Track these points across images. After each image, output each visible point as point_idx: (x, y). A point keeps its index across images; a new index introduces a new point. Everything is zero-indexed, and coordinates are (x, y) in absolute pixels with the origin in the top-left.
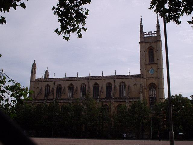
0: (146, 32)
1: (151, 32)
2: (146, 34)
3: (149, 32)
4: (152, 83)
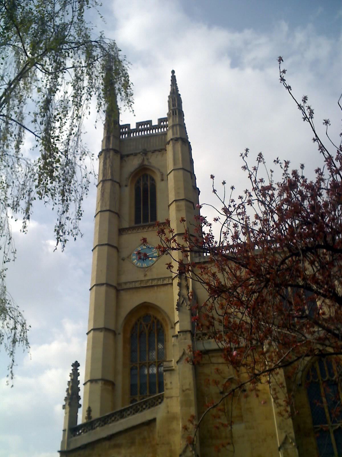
1: (150, 122)
4: (146, 306)
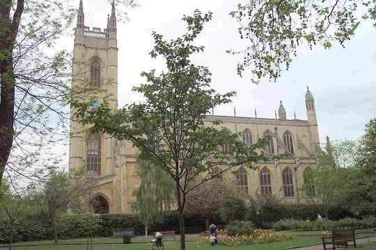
1: (99, 29)
2: (89, 32)
3: (94, 28)
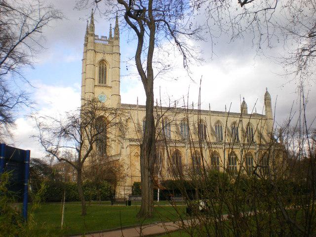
0: (97, 36)
2: (98, 39)
3: (103, 37)
